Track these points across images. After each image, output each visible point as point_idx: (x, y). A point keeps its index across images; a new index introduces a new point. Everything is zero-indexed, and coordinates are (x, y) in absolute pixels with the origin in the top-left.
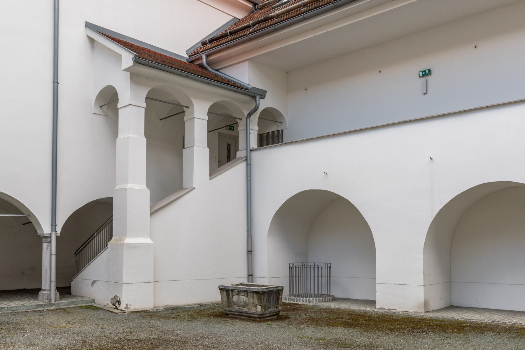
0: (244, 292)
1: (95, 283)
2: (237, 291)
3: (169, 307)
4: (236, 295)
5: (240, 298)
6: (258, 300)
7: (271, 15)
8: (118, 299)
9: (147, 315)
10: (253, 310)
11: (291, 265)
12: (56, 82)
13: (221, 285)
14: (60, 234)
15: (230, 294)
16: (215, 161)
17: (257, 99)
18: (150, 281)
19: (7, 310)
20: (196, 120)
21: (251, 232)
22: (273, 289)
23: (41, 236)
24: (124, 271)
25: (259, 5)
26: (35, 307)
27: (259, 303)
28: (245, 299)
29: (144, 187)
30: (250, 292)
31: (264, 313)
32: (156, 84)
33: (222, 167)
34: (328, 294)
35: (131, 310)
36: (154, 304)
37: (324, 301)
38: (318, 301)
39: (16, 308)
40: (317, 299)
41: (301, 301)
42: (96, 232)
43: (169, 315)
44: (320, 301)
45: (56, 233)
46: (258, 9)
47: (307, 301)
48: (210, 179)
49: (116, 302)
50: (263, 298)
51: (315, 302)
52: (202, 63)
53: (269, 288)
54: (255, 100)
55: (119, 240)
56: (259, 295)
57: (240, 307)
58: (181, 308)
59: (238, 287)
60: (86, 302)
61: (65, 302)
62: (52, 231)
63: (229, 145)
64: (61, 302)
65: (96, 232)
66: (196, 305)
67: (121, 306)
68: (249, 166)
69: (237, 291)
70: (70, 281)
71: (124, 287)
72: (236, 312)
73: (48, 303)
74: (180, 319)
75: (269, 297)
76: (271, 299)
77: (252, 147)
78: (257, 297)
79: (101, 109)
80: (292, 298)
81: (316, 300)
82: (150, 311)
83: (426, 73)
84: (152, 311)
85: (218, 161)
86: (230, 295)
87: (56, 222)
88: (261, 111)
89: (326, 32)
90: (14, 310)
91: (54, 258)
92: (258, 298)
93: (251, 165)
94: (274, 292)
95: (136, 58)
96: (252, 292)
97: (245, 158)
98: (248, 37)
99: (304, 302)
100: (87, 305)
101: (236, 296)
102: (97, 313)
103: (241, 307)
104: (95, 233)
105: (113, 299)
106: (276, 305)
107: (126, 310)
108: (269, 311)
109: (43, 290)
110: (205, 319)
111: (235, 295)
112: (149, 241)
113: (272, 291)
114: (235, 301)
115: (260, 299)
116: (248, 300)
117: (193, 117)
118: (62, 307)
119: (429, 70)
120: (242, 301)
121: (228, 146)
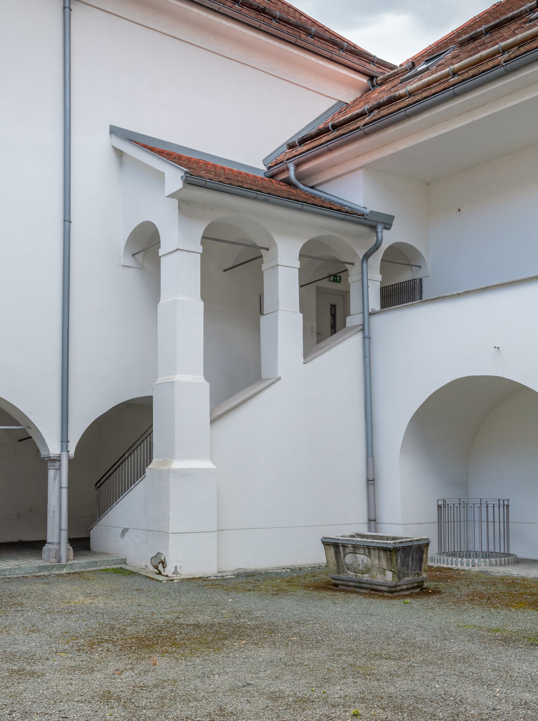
0: (364, 548)
1: (126, 532)
2: (352, 547)
5: (357, 558)
6: (388, 562)
10: (379, 578)
11: (441, 503)
12: (67, 221)
13: (325, 536)
14: (73, 456)
17: (379, 230)
21: (373, 447)
22: (412, 544)
23: (46, 459)
25: (378, 79)
26: (37, 570)
27: (388, 568)
28: (365, 561)
29: (200, 378)
30: (374, 548)
31: (398, 584)
33: (323, 343)
34: (506, 552)
35: (183, 577)
38: (488, 563)
39: (10, 572)
40: (487, 560)
41: (459, 564)
42: (127, 451)
45: (68, 454)
48: (304, 363)
51: (483, 565)
52: (288, 178)
53: (405, 542)
54: (375, 231)
56: (389, 553)
62: (62, 450)
64: (76, 561)
65: (127, 451)
67: (166, 569)
68: (367, 339)
69: (352, 547)
70: (89, 529)
71: (172, 539)
72: (351, 581)
75: (405, 557)
76: (408, 561)
78: (385, 556)
79: (135, 258)
81: (485, 562)
82: (212, 578)
84: (215, 578)
86: (340, 553)
87: (67, 437)
91: (65, 492)
92: (387, 559)
95: (186, 176)
96: (378, 549)
97: (361, 327)
99: (465, 565)
101: (351, 554)
102: (130, 580)
104: (125, 453)
105: (155, 557)
106: (418, 571)
107: (175, 577)
109: (49, 543)
112: (208, 465)
113: (411, 547)
114: (348, 563)
118: (77, 570)
120: (360, 563)
121: (331, 309)
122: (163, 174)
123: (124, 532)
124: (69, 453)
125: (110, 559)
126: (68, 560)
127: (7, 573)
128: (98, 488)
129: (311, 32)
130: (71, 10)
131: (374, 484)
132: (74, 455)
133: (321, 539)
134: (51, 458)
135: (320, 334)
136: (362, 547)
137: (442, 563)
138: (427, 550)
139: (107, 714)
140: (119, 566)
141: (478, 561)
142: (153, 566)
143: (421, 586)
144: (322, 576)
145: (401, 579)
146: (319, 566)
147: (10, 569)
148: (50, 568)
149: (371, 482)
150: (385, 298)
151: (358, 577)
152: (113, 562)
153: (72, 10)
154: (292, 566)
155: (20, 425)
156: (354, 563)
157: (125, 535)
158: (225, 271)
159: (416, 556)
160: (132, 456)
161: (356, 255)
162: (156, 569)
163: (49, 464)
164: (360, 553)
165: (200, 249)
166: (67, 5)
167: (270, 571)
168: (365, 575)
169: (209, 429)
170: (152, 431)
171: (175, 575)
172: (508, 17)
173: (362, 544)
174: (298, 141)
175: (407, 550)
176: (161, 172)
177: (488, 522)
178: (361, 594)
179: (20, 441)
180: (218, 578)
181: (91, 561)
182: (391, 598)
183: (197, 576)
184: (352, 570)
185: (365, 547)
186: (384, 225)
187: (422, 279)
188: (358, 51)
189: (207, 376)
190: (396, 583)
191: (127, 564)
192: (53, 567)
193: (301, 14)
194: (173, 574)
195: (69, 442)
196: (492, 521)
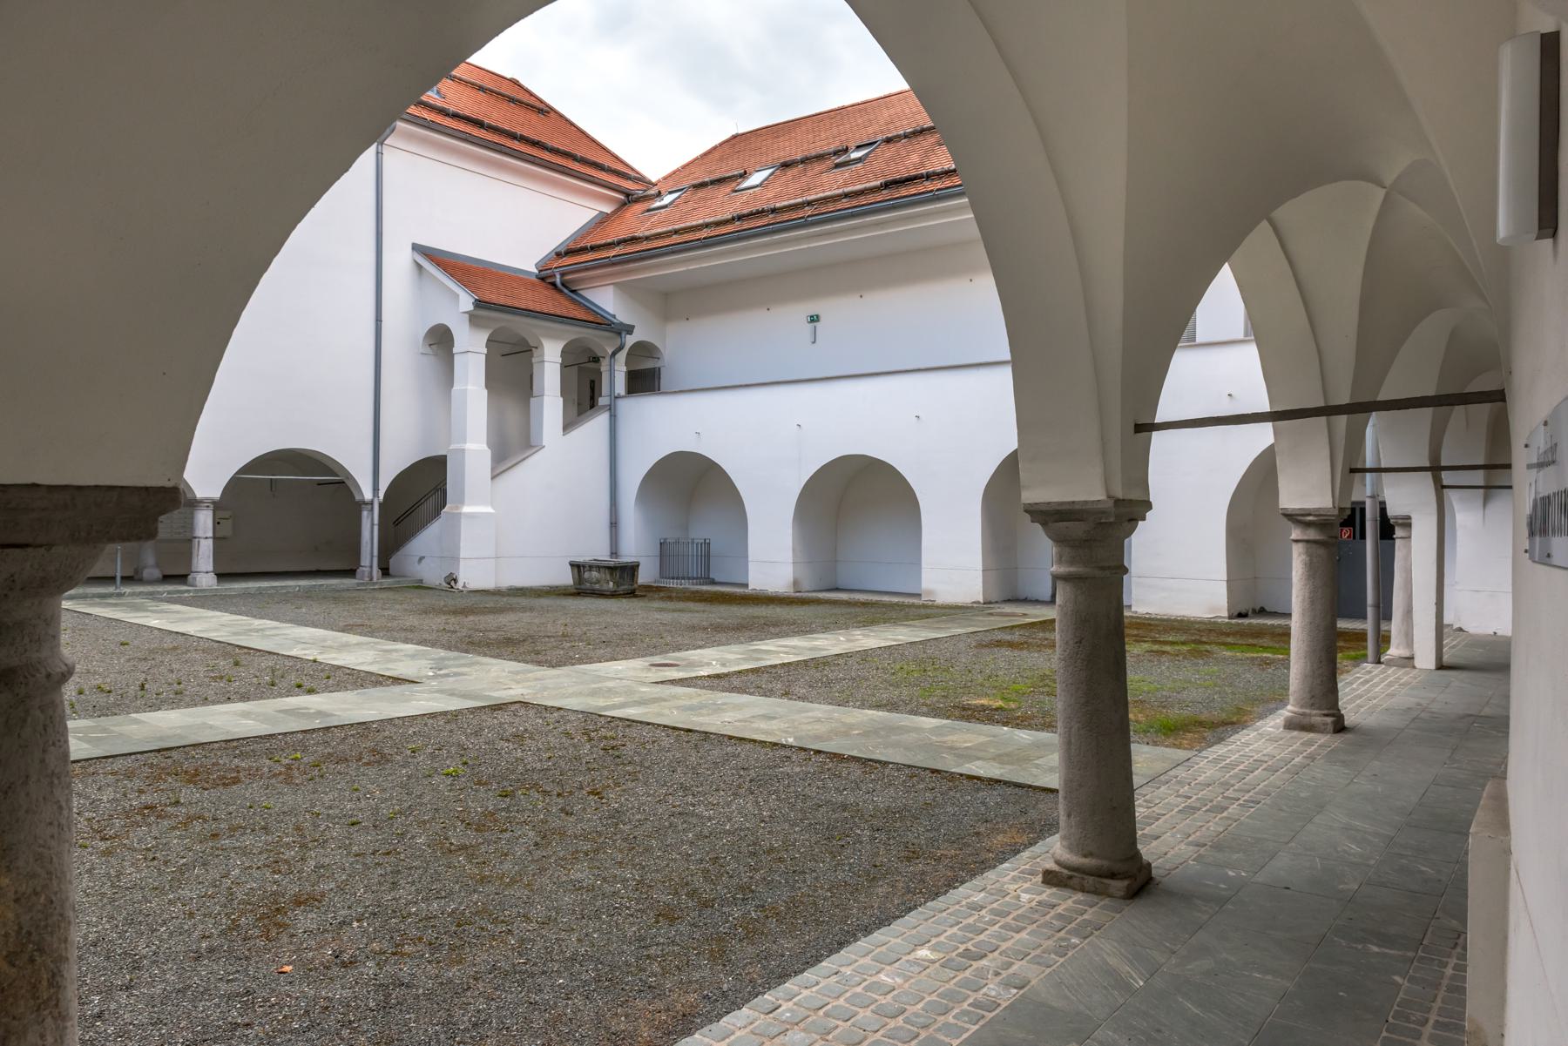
10: (605, 587)
17: (623, 336)
20: (546, 363)
29: (485, 447)
33: (582, 416)
49: (452, 580)
61: (388, 581)
62: (374, 496)
71: (462, 563)
83: (814, 319)
91: (376, 528)
107: (463, 589)
110: (554, 597)
119: (817, 316)
122: (458, 296)
126: (378, 579)
139: (300, 931)
165: (485, 351)
179: (319, 484)
189: (489, 448)
192: (367, 584)
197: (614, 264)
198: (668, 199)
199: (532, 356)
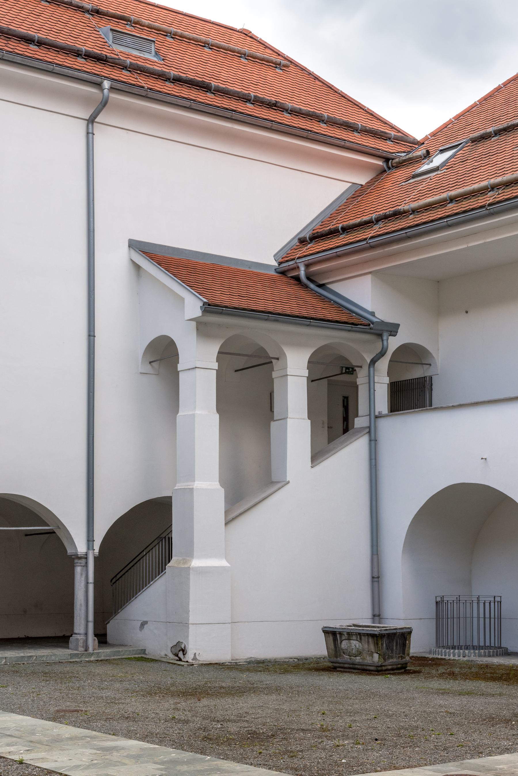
0: (356, 635)
1: (145, 625)
2: (346, 634)
3: (253, 660)
4: (346, 639)
5: (351, 643)
7: (404, 209)
8: (183, 646)
9: (224, 668)
10: (368, 660)
12: (91, 335)
13: (325, 626)
14: (98, 554)
15: (337, 638)
16: (322, 427)
17: (385, 338)
18: (227, 622)
19: (36, 660)
21: (377, 546)
22: (395, 632)
23: (73, 557)
24: (191, 607)
25: (394, 161)
26: (69, 657)
27: (375, 651)
28: (357, 645)
30: (365, 634)
31: (383, 664)
32: (230, 333)
34: (499, 646)
35: (201, 663)
36: (232, 655)
37: (487, 654)
38: (477, 654)
39: (47, 658)
40: (477, 651)
41: (452, 655)
42: (145, 549)
43: (255, 668)
44: (481, 654)
45: (94, 553)
46: (393, 166)
47: (460, 654)
48: (312, 467)
50: (382, 644)
51: (472, 656)
53: (390, 629)
54: (381, 338)
55: (182, 562)
56: (375, 638)
57: (351, 656)
58: (270, 662)
59: (349, 629)
60: (134, 652)
61: (105, 652)
62: (88, 549)
63: (346, 399)
64: (100, 651)
65: (145, 549)
66: (292, 658)
67: (186, 656)
69: (346, 634)
70: (106, 623)
71: (191, 628)
72: (346, 664)
73: (86, 652)
74: (270, 672)
75: (390, 642)
76: (393, 646)
77: (379, 412)
78: (373, 641)
79: (151, 365)
80: (438, 650)
81: (475, 653)
82: (227, 664)
84: (229, 664)
85: (328, 427)
86: (337, 640)
87: (93, 537)
88: (392, 352)
89: (483, 243)
90: (44, 660)
91: (91, 587)
92: (375, 643)
93: (376, 441)
94: (398, 636)
95: (205, 307)
96: (367, 635)
97: (367, 430)
98: (368, 244)
99: (457, 656)
100: (137, 656)
101: (346, 640)
102: (156, 665)
103: (353, 656)
104: (143, 551)
105: (175, 647)
106: (401, 655)
107: (194, 662)
108: (390, 662)
109: (76, 634)
111: (344, 640)
112: (224, 563)
113: (395, 634)
114: (344, 648)
115: (377, 644)
116: (362, 646)
117: (285, 374)
118: (103, 658)
120: (353, 648)
121: (343, 401)
123: (143, 625)
124: (95, 551)
125: (131, 649)
127: (44, 659)
128: (114, 583)
129: (323, 118)
130: (94, 134)
131: (378, 581)
132: (99, 553)
133: (322, 628)
134: (79, 556)
135: (332, 427)
136: (355, 634)
137: (437, 655)
138: (410, 638)
140: (140, 656)
141: (469, 652)
142: (173, 654)
143: (405, 668)
144: (325, 663)
145: (386, 660)
146: (324, 657)
147: (47, 655)
148: (80, 656)
149: (376, 579)
150: (397, 393)
151: (352, 659)
152: (134, 652)
153: (95, 135)
154: (299, 657)
155: (48, 526)
156: (348, 647)
157: (144, 628)
158: (236, 371)
159: (400, 642)
160: (150, 553)
161: (364, 359)
162: (176, 656)
163: (76, 561)
164: (353, 639)
166: (90, 131)
167: (279, 660)
168: (358, 658)
169: (224, 531)
170: (171, 531)
171: (194, 661)
172: (515, 124)
173: (354, 632)
174: (309, 238)
175: (391, 636)
176: (181, 297)
177: (490, 618)
178: (354, 673)
180: (232, 664)
181: (114, 650)
182: (377, 675)
183: (213, 662)
184: (347, 654)
185: (357, 634)
186: (389, 332)
187: (432, 376)
188: (374, 131)
190: (382, 663)
191: (146, 654)
192: (82, 655)
193: (315, 77)
194: (193, 660)
195: (94, 541)
196: (494, 617)
197: (372, 247)
198: (438, 160)
199: (272, 370)
